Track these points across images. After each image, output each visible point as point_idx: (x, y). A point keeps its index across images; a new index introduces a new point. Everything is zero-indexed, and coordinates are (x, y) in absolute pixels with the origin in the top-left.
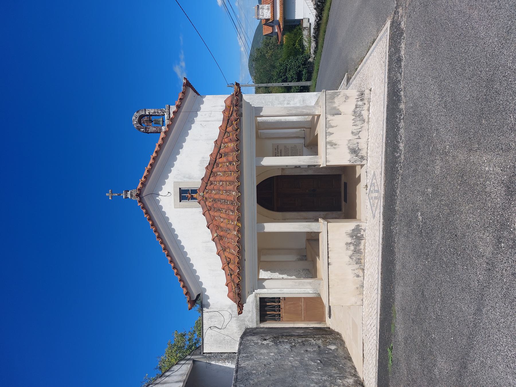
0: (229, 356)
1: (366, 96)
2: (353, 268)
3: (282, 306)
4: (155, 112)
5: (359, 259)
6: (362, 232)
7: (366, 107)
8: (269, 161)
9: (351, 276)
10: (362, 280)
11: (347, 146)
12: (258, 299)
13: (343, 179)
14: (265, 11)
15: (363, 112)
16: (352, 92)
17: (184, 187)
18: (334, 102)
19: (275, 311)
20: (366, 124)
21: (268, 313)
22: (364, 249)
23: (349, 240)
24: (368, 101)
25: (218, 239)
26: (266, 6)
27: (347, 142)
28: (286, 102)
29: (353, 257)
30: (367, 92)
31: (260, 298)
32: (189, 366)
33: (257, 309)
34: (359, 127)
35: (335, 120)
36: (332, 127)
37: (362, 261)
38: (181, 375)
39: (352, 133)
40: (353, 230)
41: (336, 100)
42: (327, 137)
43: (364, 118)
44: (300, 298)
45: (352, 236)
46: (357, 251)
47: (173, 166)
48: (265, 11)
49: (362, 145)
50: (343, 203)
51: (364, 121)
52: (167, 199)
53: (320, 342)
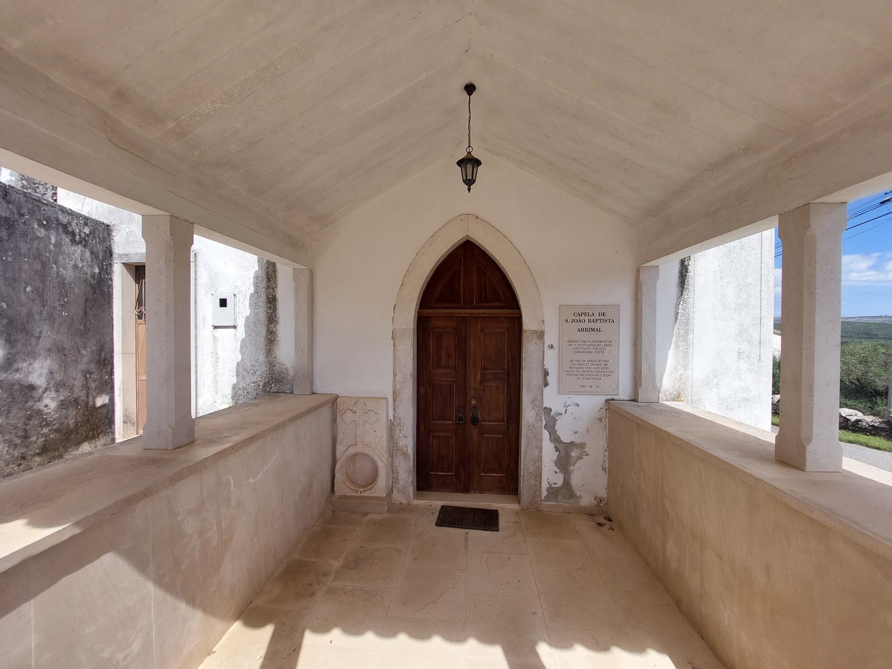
13: (504, 506)
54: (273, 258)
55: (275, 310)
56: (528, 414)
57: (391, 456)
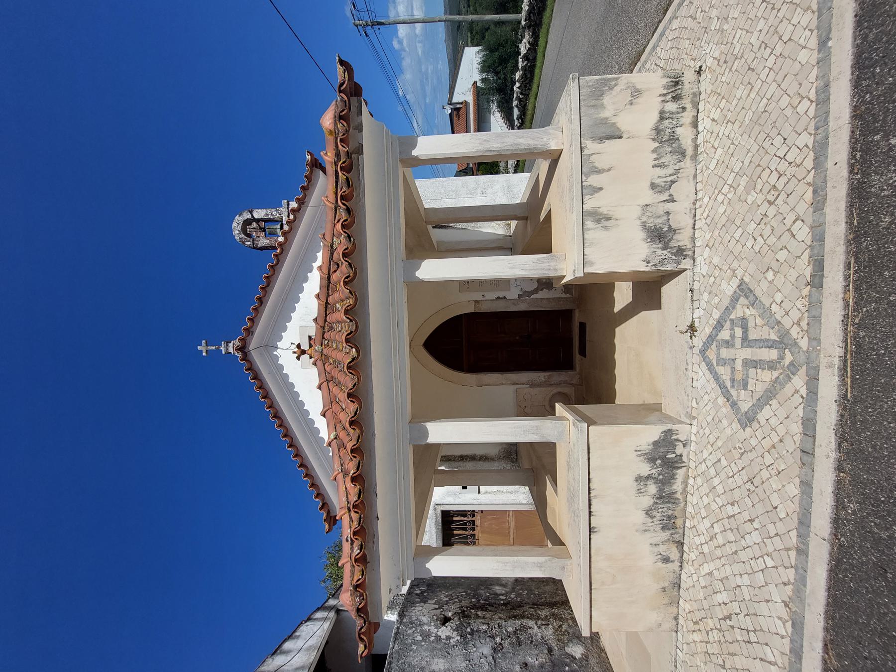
1: (687, 88)
2: (654, 541)
3: (478, 522)
4: (267, 215)
5: (669, 517)
6: (679, 449)
7: (687, 117)
8: (432, 270)
9: (647, 559)
10: (677, 569)
11: (639, 222)
12: (439, 513)
13: (577, 318)
15: (679, 131)
16: (650, 79)
18: (603, 106)
19: (465, 529)
20: (688, 163)
21: (455, 532)
22: (685, 491)
23: (645, 469)
24: (692, 102)
27: (638, 211)
28: (479, 191)
29: (655, 513)
30: (689, 76)
31: (443, 512)
32: (327, 626)
33: (437, 529)
34: (670, 170)
35: (607, 153)
36: (599, 171)
37: (679, 522)
38: (309, 649)
39: (653, 186)
40: (656, 443)
41: (607, 100)
42: (586, 198)
43: (684, 146)
44: (506, 512)
45: (652, 460)
46: (665, 497)
47: (298, 300)
49: (681, 218)
50: (577, 357)
51: (683, 154)
52: (285, 356)
53: (549, 632)
54: (439, 458)
55: (467, 456)
56: (522, 307)
57: (551, 385)
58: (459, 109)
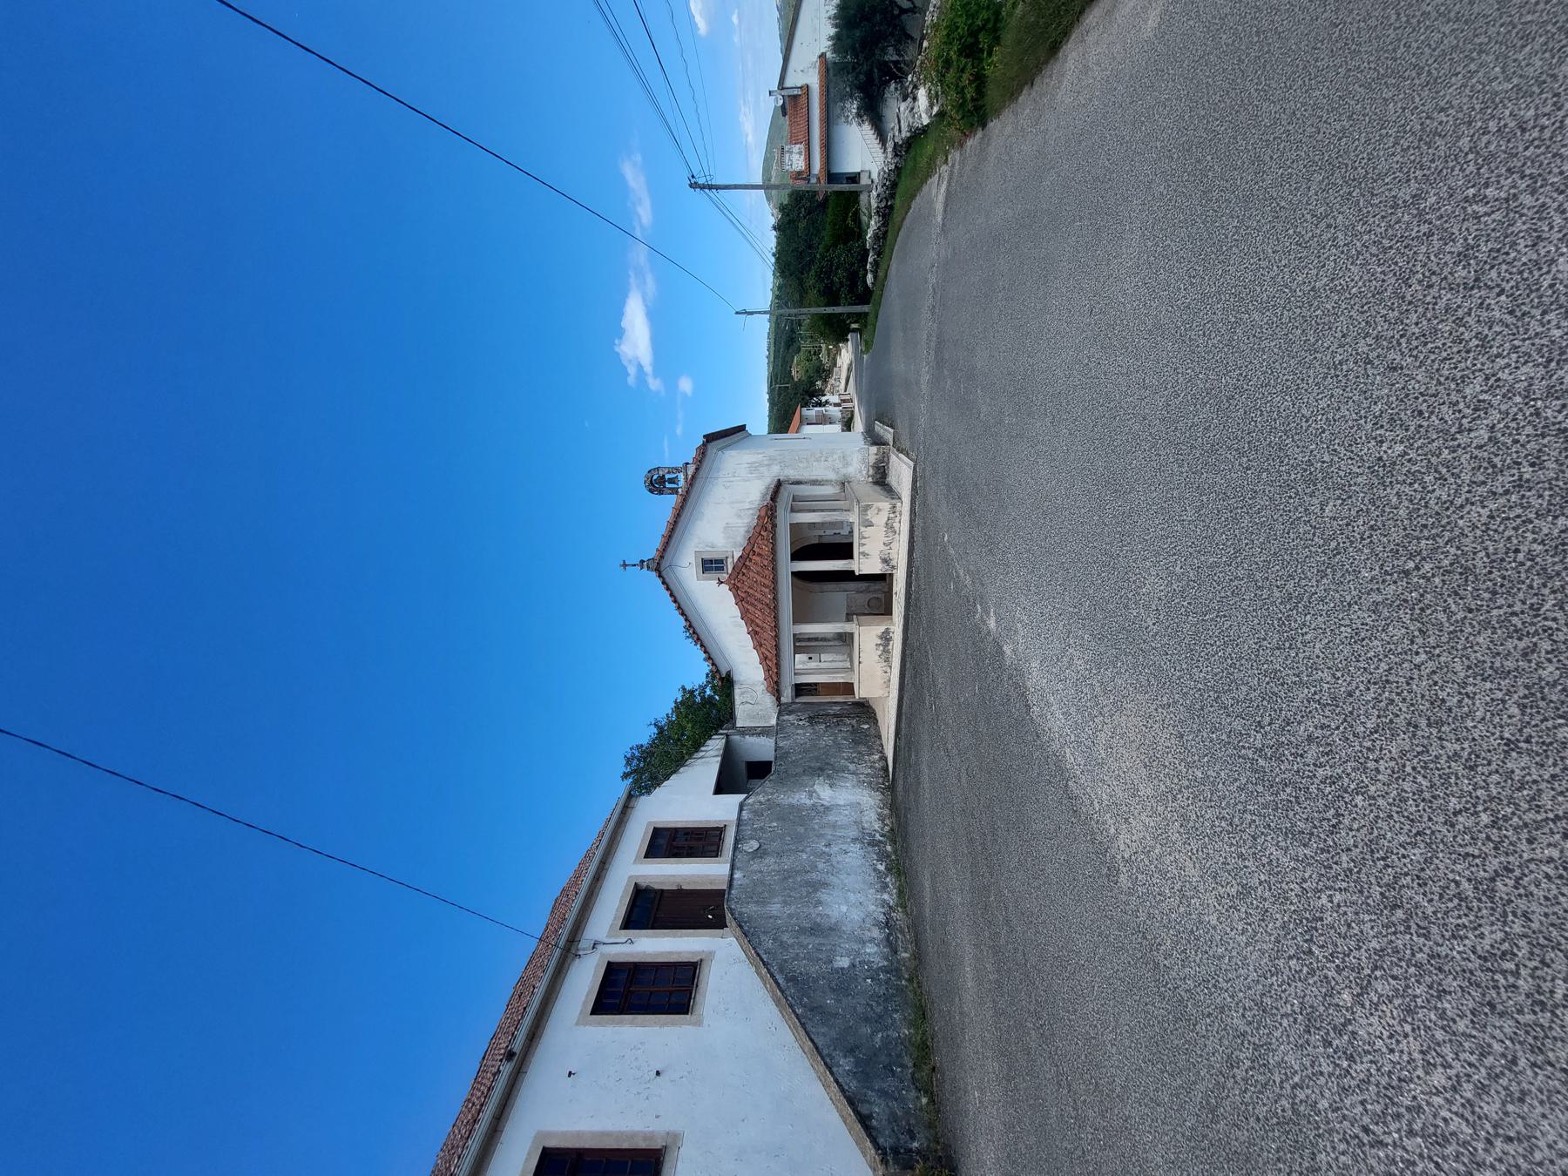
0: (764, 732)
9: (879, 672)
14: (795, 157)
17: (707, 557)
25: (754, 634)
26: (796, 148)
35: (867, 531)
48: (795, 157)
58: (795, 97)
